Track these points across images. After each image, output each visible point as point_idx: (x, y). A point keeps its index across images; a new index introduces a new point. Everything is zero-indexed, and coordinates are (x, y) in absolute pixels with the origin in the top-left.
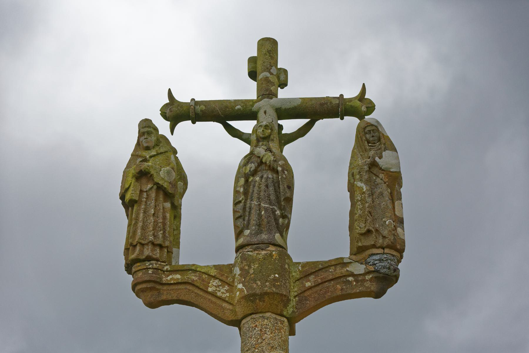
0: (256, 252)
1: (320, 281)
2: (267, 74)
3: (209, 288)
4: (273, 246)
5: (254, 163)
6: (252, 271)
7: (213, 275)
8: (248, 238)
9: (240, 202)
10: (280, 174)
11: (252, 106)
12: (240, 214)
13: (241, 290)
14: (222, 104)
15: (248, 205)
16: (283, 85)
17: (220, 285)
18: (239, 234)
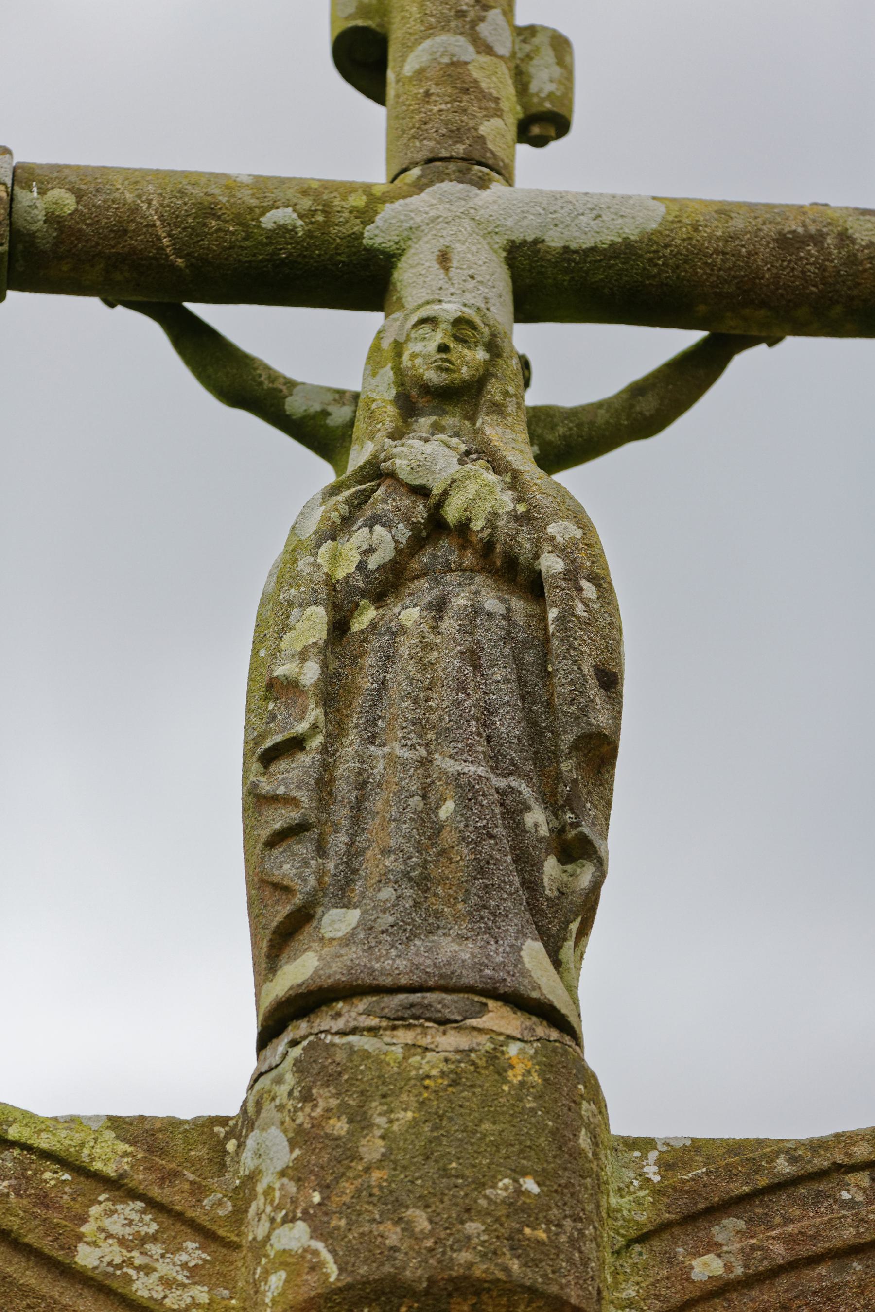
0: (405, 1036)
1: (779, 1251)
2: (459, 46)
3: (82, 1248)
4: (506, 1011)
5: (388, 526)
6: (372, 1148)
7: (110, 1170)
8: (354, 954)
9: (297, 744)
10: (551, 595)
11: (366, 215)
12: (293, 815)
13: (299, 1263)
14: (182, 193)
15: (347, 765)
16: (544, 124)
17: (154, 1238)
18: (280, 934)
